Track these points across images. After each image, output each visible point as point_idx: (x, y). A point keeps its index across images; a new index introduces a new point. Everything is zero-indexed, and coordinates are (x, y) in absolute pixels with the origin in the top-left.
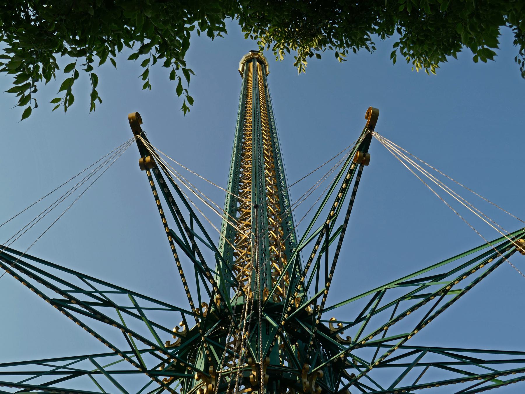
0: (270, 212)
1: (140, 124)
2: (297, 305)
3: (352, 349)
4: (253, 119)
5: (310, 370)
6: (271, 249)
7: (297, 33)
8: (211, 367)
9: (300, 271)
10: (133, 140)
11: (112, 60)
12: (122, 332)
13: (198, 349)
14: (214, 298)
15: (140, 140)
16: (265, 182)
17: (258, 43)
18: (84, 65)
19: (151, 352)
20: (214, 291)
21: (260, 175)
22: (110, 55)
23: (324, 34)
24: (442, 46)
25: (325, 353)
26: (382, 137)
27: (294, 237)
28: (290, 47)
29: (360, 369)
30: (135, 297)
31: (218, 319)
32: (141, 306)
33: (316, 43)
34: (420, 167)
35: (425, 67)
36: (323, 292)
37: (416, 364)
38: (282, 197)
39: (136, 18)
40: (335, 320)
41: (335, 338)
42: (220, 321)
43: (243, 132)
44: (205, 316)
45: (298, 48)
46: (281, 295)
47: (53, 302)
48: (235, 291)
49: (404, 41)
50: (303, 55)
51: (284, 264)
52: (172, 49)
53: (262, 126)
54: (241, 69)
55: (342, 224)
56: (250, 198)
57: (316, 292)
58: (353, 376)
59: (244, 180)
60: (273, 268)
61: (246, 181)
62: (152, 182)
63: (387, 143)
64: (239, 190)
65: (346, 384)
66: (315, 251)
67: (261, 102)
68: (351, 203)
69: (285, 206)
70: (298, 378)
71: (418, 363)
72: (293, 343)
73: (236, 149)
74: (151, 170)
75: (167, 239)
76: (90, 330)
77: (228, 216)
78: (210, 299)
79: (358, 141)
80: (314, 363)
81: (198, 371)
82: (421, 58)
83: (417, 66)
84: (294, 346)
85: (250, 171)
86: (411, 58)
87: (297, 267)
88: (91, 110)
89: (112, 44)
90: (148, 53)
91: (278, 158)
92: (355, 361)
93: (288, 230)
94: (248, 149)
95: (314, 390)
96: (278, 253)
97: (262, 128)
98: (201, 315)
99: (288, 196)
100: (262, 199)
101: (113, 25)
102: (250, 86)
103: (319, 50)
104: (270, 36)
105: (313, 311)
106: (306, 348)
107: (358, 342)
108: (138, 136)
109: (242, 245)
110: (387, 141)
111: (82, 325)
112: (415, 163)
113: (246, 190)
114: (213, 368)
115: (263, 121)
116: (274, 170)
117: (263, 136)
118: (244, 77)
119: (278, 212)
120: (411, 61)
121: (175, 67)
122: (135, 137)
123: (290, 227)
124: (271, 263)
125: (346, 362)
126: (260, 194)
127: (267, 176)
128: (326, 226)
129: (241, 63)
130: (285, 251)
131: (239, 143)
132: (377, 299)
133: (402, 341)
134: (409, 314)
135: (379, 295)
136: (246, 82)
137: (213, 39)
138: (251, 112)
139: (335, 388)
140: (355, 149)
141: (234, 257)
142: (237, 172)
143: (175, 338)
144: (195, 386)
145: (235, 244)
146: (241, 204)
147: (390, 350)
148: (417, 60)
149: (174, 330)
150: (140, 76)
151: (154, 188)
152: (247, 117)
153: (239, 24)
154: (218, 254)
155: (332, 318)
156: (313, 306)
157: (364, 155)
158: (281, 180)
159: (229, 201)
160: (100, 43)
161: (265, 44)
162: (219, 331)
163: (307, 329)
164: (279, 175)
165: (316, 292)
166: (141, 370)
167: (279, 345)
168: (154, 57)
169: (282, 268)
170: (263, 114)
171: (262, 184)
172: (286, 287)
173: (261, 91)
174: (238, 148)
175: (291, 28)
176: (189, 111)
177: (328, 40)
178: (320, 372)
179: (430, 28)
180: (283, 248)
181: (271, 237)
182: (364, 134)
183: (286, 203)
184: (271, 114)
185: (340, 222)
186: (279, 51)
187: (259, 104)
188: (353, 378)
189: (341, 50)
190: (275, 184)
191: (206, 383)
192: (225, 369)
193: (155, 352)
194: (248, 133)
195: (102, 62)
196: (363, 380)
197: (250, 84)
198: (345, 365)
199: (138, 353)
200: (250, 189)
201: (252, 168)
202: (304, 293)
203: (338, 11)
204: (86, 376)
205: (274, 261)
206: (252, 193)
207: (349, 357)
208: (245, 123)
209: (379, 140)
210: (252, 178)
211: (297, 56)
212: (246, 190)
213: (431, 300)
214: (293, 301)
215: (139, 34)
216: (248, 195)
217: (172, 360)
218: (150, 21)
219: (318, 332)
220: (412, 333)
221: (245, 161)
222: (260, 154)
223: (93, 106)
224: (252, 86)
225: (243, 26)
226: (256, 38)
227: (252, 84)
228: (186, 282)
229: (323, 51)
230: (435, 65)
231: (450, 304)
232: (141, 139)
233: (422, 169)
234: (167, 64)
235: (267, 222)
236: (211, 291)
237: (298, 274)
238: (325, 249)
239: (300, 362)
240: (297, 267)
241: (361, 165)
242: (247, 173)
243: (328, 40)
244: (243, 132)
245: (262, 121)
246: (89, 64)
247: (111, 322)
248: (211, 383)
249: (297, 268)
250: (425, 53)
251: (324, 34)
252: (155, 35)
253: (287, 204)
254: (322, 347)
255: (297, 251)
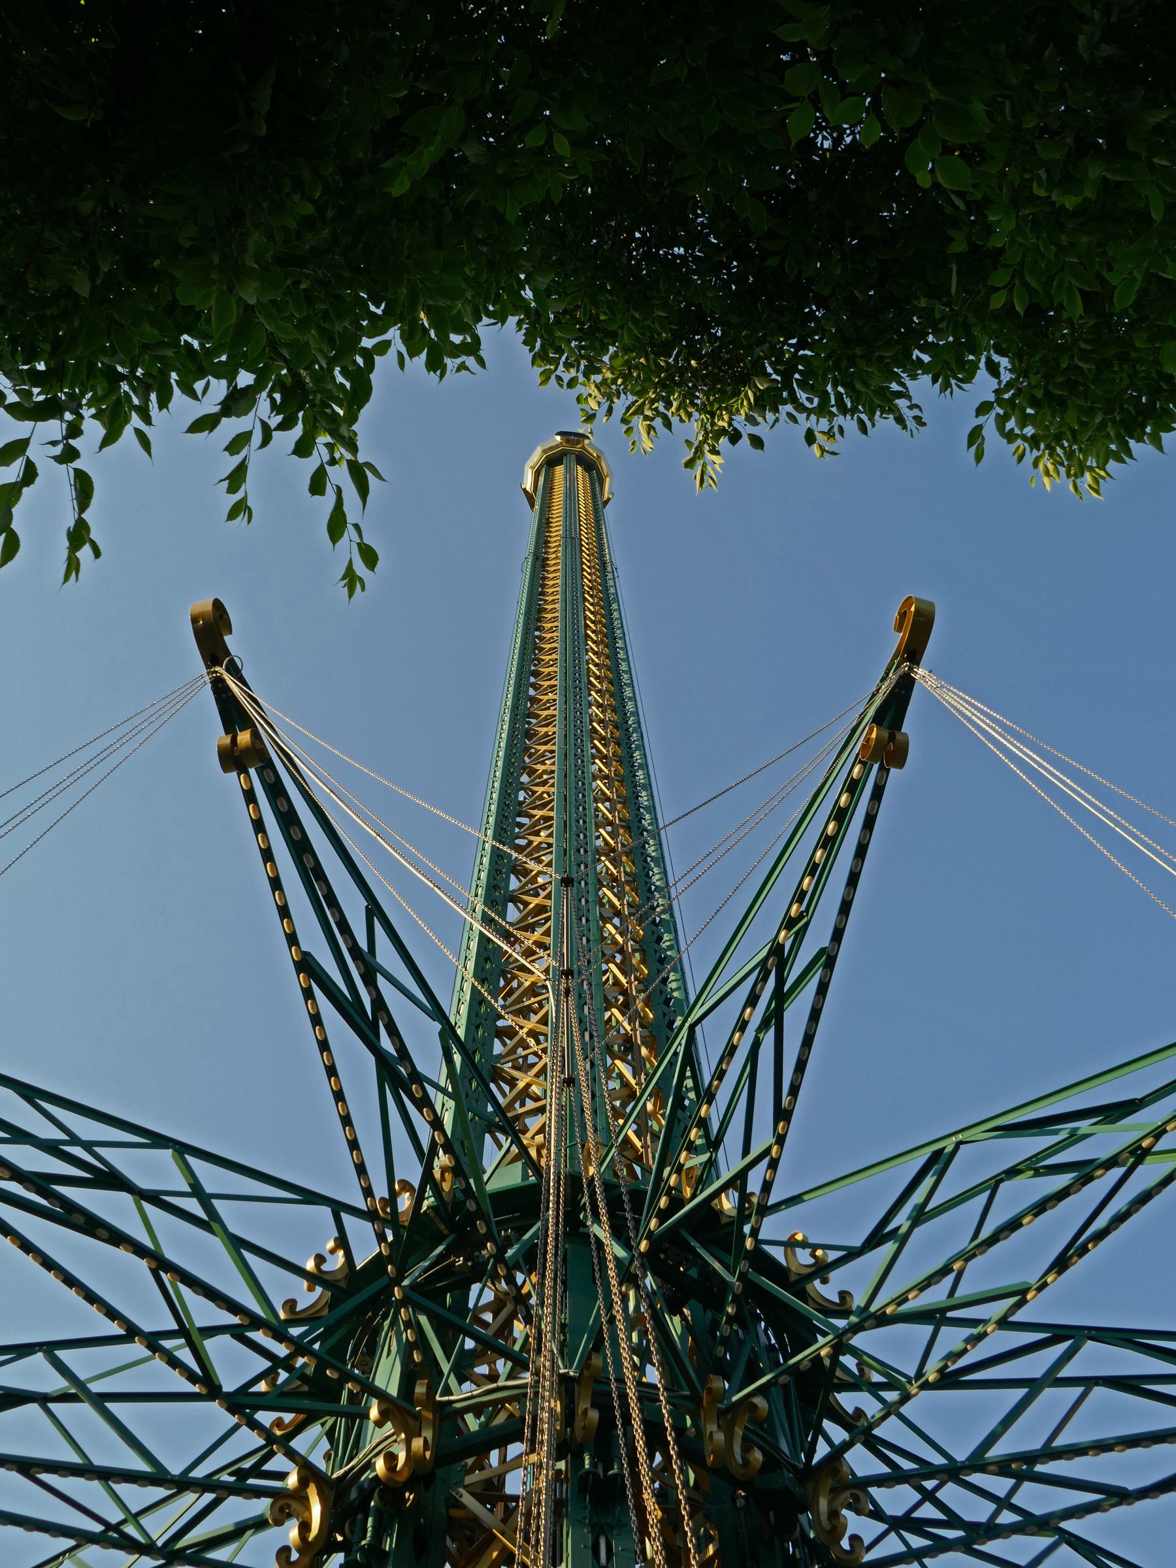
0: (607, 906)
1: (226, 635)
2: (688, 1192)
3: (855, 1329)
4: (561, 630)
5: (726, 1394)
6: (610, 1018)
7: (695, 372)
8: (420, 1384)
9: (696, 1088)
10: (202, 681)
11: (139, 433)
12: (150, 1268)
13: (381, 1325)
14: (435, 1166)
15: (224, 681)
16: (593, 816)
17: (579, 400)
18: (54, 443)
19: (237, 1333)
20: (433, 1144)
21: (580, 772)
22: (136, 421)
23: (774, 376)
24: (1119, 413)
25: (773, 1341)
26: (943, 683)
27: (680, 983)
28: (673, 413)
29: (881, 1393)
30: (192, 1161)
31: (446, 1232)
32: (209, 1189)
33: (749, 403)
34: (1058, 774)
35: (1068, 475)
36: (767, 1152)
37: (1052, 1379)
38: (645, 860)
39: (213, 302)
40: (803, 1241)
41: (804, 1296)
42: (449, 1240)
43: (533, 668)
44: (406, 1224)
45: (696, 415)
46: (639, 1159)
48: (500, 1146)
49: (1006, 396)
50: (711, 435)
51: (648, 1066)
52: (317, 402)
53: (587, 651)
54: (528, 485)
55: (826, 942)
56: (549, 864)
57: (746, 1151)
58: (860, 1417)
59: (533, 808)
60: (614, 1075)
61: (539, 813)
62: (253, 807)
63: (958, 702)
64: (516, 839)
65: (837, 1441)
66: (742, 1026)
67: (585, 580)
68: (853, 880)
69: (653, 888)
70: (689, 1422)
71: (1058, 1376)
72: (675, 1310)
73: (509, 715)
74: (252, 771)
75: (294, 982)
76: (48, 1264)
77: (483, 910)
78: (419, 1170)
79: (874, 695)
80: (739, 1374)
81: (381, 1395)
82: (1059, 450)
83: (1047, 473)
84: (677, 1319)
85: (551, 781)
86: (1028, 449)
87: (688, 1074)
88: (67, 577)
89: (143, 388)
90: (246, 414)
91: (633, 746)
92: (866, 1369)
93: (662, 961)
94: (546, 718)
95: (739, 1460)
96: (631, 1030)
97: (587, 657)
98: (393, 1220)
99: (663, 857)
100: (586, 866)
101: (147, 328)
102: (555, 534)
103: (756, 423)
104: (614, 381)
105: (736, 1211)
106: (715, 1325)
107: (873, 1309)
108: (218, 669)
109: (521, 1005)
110: (962, 698)
111: (27, 1246)
112: (1045, 764)
113: (536, 840)
114: (429, 1387)
115: (593, 636)
116: (621, 781)
117: (592, 679)
118: (537, 507)
119: (632, 907)
120: (1030, 457)
121: (326, 458)
122: (208, 673)
123: (669, 953)
124: (609, 1061)
125: (838, 1373)
126: (578, 851)
127: (600, 799)
128: (777, 950)
129: (531, 468)
130: (651, 1025)
131: (519, 700)
132: (932, 1176)
133: (1008, 1306)
134: (1030, 1222)
135: (939, 1162)
136: (545, 523)
137: (442, 376)
138: (555, 609)
139: (802, 1455)
140: (864, 718)
141: (496, 1041)
142: (511, 784)
143: (310, 1289)
144: (370, 1442)
145: (501, 1002)
146: (520, 881)
147: (972, 1335)
148: (1047, 456)
149: (310, 1265)
150: (221, 481)
151: (259, 826)
152: (546, 622)
153: (525, 343)
154: (448, 1031)
155: (795, 1234)
156: (736, 1195)
157: (892, 738)
158: (641, 810)
159: (486, 871)
160: (106, 385)
161: (599, 403)
162: (449, 1270)
163: (717, 1266)
164: (637, 797)
165: (746, 1151)
166: (204, 1392)
167: (632, 1316)
168: (265, 426)
169: (643, 1077)
170: (592, 616)
171: (585, 822)
172: (655, 1136)
173: (587, 549)
174: (517, 715)
175: (676, 360)
176: (363, 589)
177: (784, 393)
178: (759, 1401)
179: (1080, 364)
180: (646, 1014)
181: (611, 982)
182: (890, 675)
183: (657, 880)
184: (616, 614)
185: (817, 938)
186: (640, 424)
187: (579, 587)
188: (859, 1424)
189: (824, 424)
190: (624, 824)
191: (403, 1436)
192: (464, 1391)
193: (248, 1334)
194: (547, 670)
195: (109, 439)
196: (889, 1430)
197: (555, 529)
198: (835, 1381)
199: (195, 1336)
200: (550, 835)
201: (556, 775)
202: (709, 1154)
203: (815, 311)
204: (33, 1408)
205: (620, 1055)
206: (554, 849)
207: (848, 1356)
208: (537, 641)
209: (937, 693)
210: (554, 803)
211: (692, 439)
212: (536, 840)
213: (1096, 1180)
214: (674, 1177)
215: (224, 358)
216: (542, 853)
217: (300, 1361)
218: (257, 320)
219: (752, 1275)
220: (1039, 1281)
221: (536, 753)
222: (582, 731)
223: (74, 566)
224: (561, 533)
225: (536, 350)
226: (572, 383)
227: (561, 528)
228: (348, 1115)
229: (771, 424)
230: (1097, 470)
231: (1153, 1192)
232: (226, 678)
233: (1065, 779)
234: (303, 448)
235: (598, 937)
236: (425, 1146)
237: (692, 1095)
238: (774, 1018)
239: (695, 1371)
240: (688, 1074)
241: (881, 768)
242: (540, 790)
243: (785, 394)
244: (533, 668)
245: (587, 636)
246: (67, 442)
247: (116, 1238)
248: (420, 1436)
249: (688, 1078)
250: (1068, 433)
251: (774, 376)
252: (271, 362)
253: (658, 883)
254: (763, 1324)
255: (687, 1025)
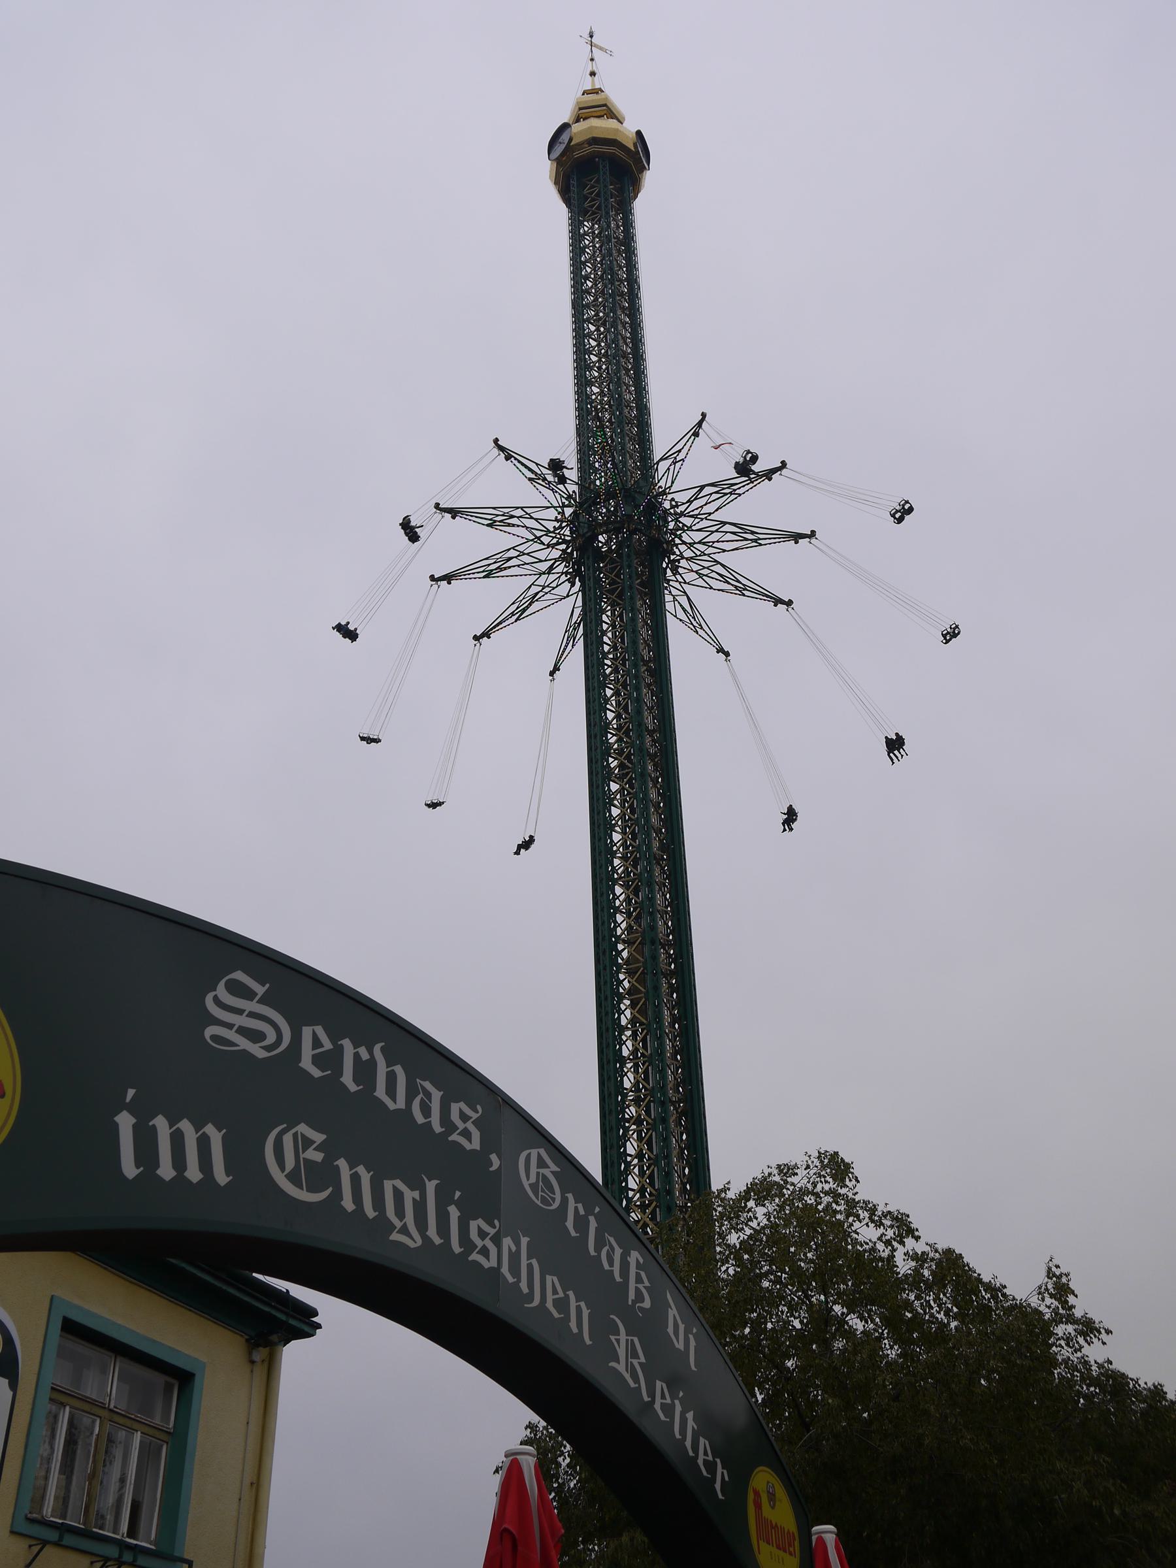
19: (546, 535)
47: (484, 577)
204: (515, 559)
247: (513, 525)
